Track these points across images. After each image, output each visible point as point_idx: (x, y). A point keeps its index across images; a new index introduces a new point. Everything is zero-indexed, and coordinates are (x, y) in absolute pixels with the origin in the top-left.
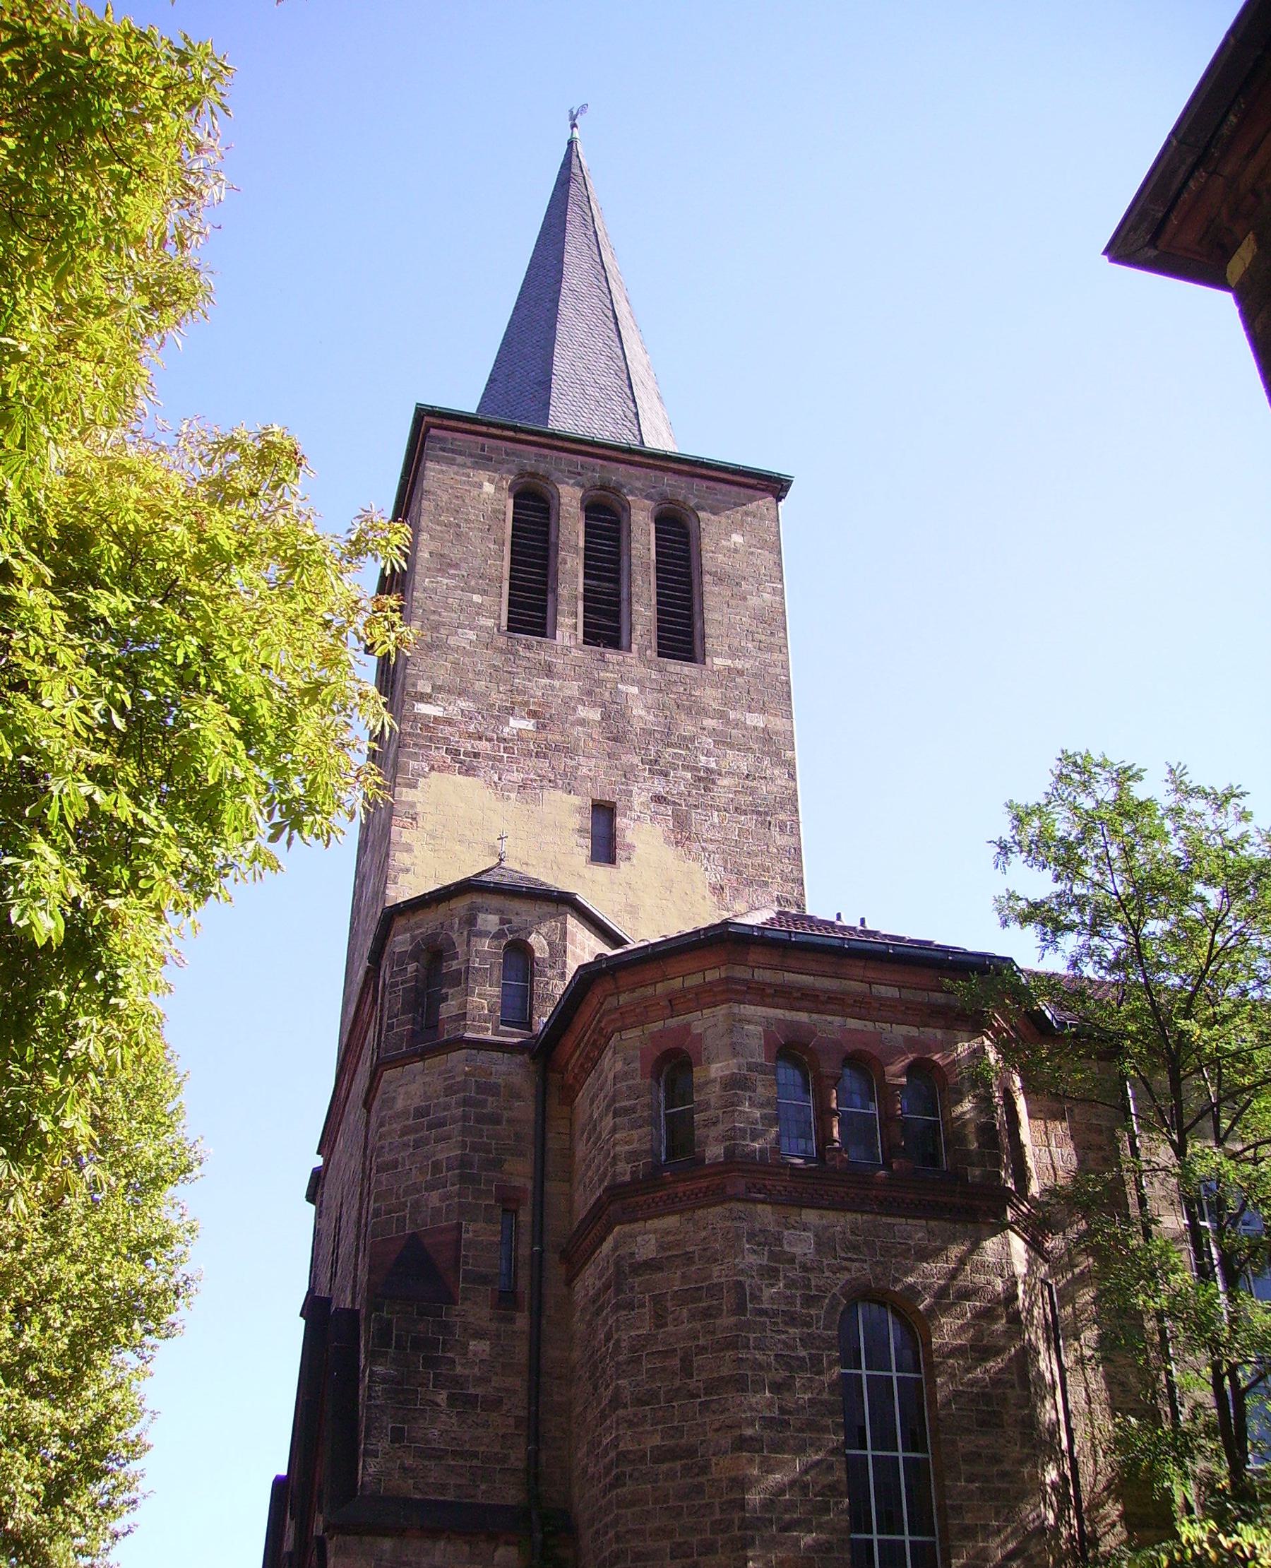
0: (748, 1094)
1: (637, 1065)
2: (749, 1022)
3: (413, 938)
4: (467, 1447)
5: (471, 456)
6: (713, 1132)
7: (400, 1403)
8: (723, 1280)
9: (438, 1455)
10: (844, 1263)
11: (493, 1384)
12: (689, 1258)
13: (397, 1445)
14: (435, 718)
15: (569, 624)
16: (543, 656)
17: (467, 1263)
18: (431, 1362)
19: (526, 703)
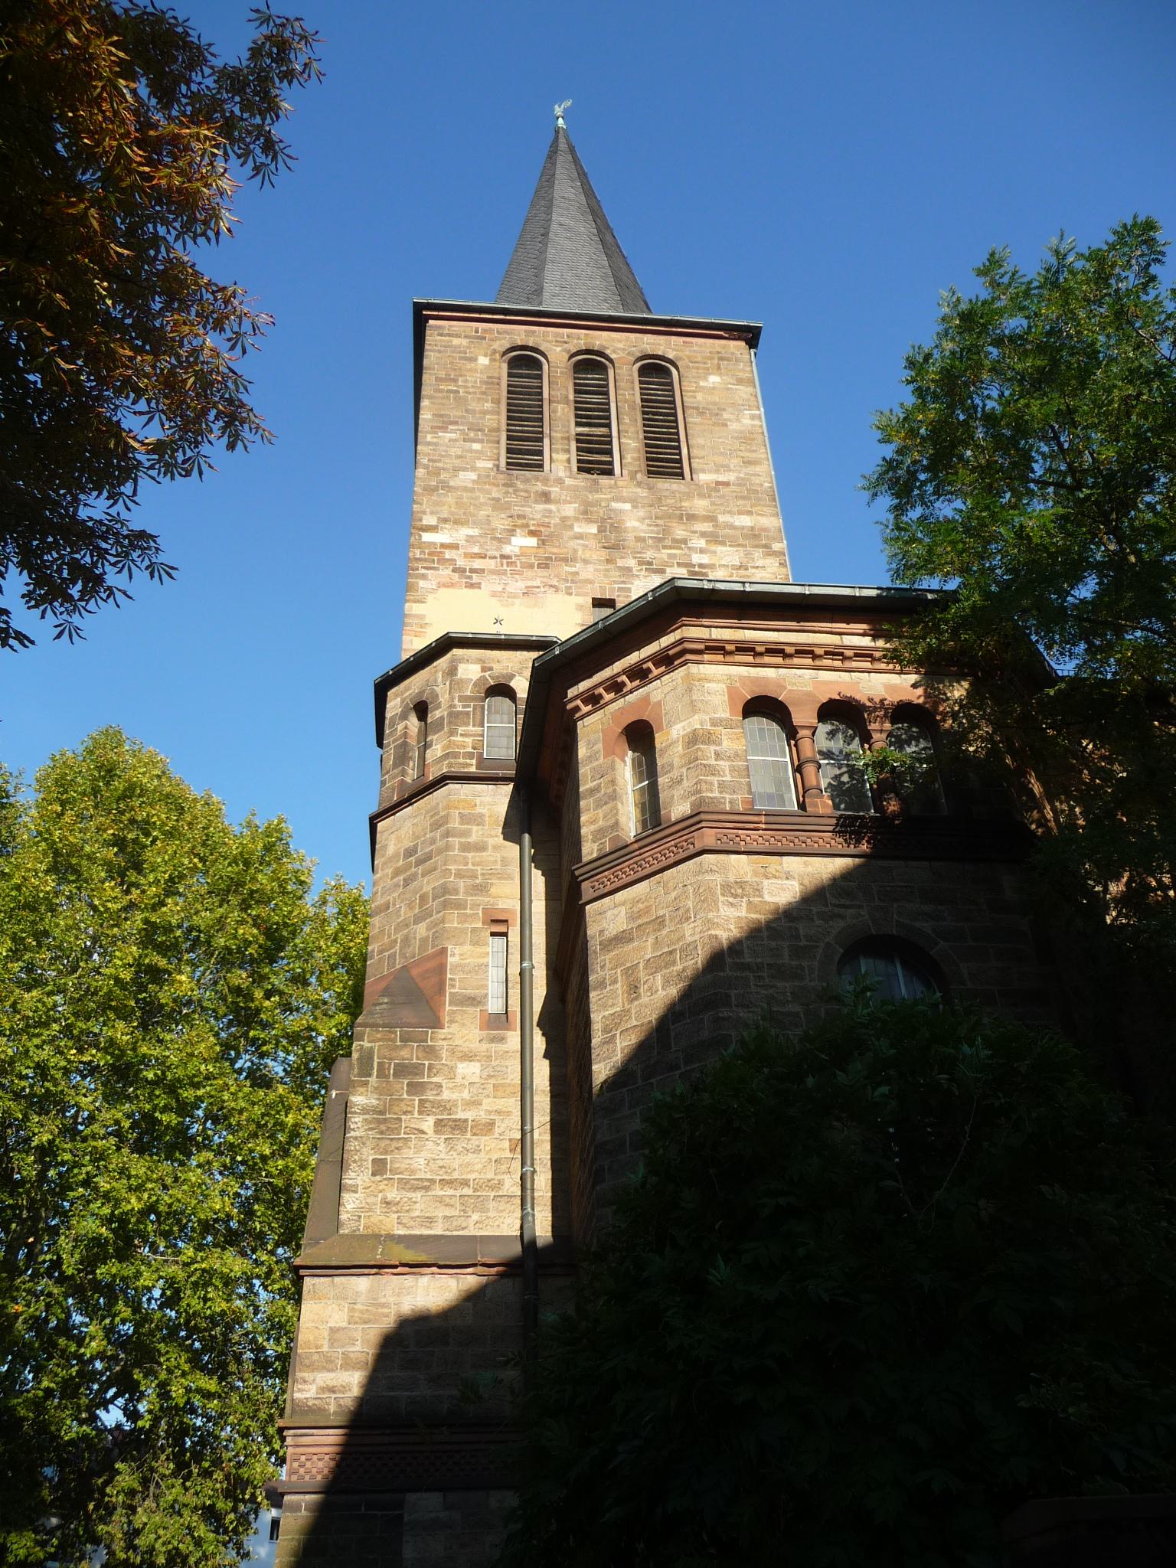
0: (713, 748)
1: (600, 746)
2: (710, 681)
3: (402, 701)
4: (455, 1175)
5: (466, 337)
6: (678, 792)
7: (382, 1133)
8: (697, 937)
9: (425, 1186)
10: (836, 910)
11: (484, 1107)
12: (660, 922)
13: (378, 1178)
14: (443, 546)
15: (560, 459)
16: (540, 487)
17: (453, 986)
18: (415, 1088)
19: (527, 525)
